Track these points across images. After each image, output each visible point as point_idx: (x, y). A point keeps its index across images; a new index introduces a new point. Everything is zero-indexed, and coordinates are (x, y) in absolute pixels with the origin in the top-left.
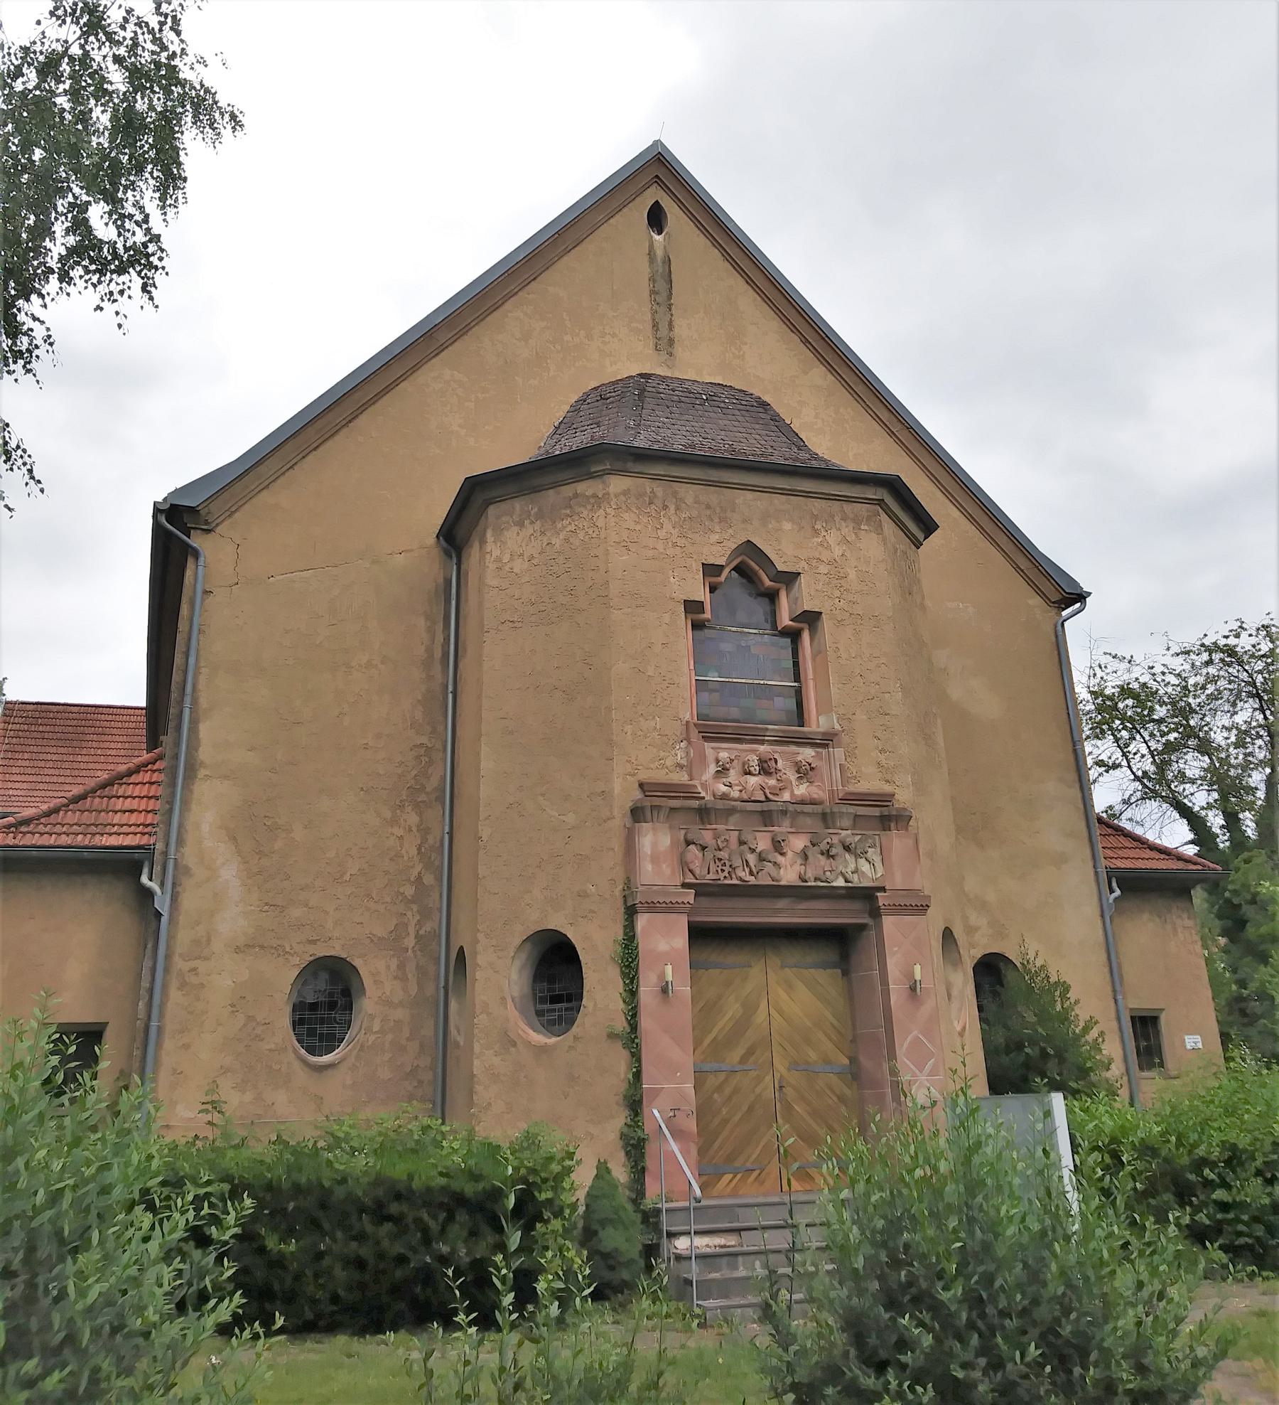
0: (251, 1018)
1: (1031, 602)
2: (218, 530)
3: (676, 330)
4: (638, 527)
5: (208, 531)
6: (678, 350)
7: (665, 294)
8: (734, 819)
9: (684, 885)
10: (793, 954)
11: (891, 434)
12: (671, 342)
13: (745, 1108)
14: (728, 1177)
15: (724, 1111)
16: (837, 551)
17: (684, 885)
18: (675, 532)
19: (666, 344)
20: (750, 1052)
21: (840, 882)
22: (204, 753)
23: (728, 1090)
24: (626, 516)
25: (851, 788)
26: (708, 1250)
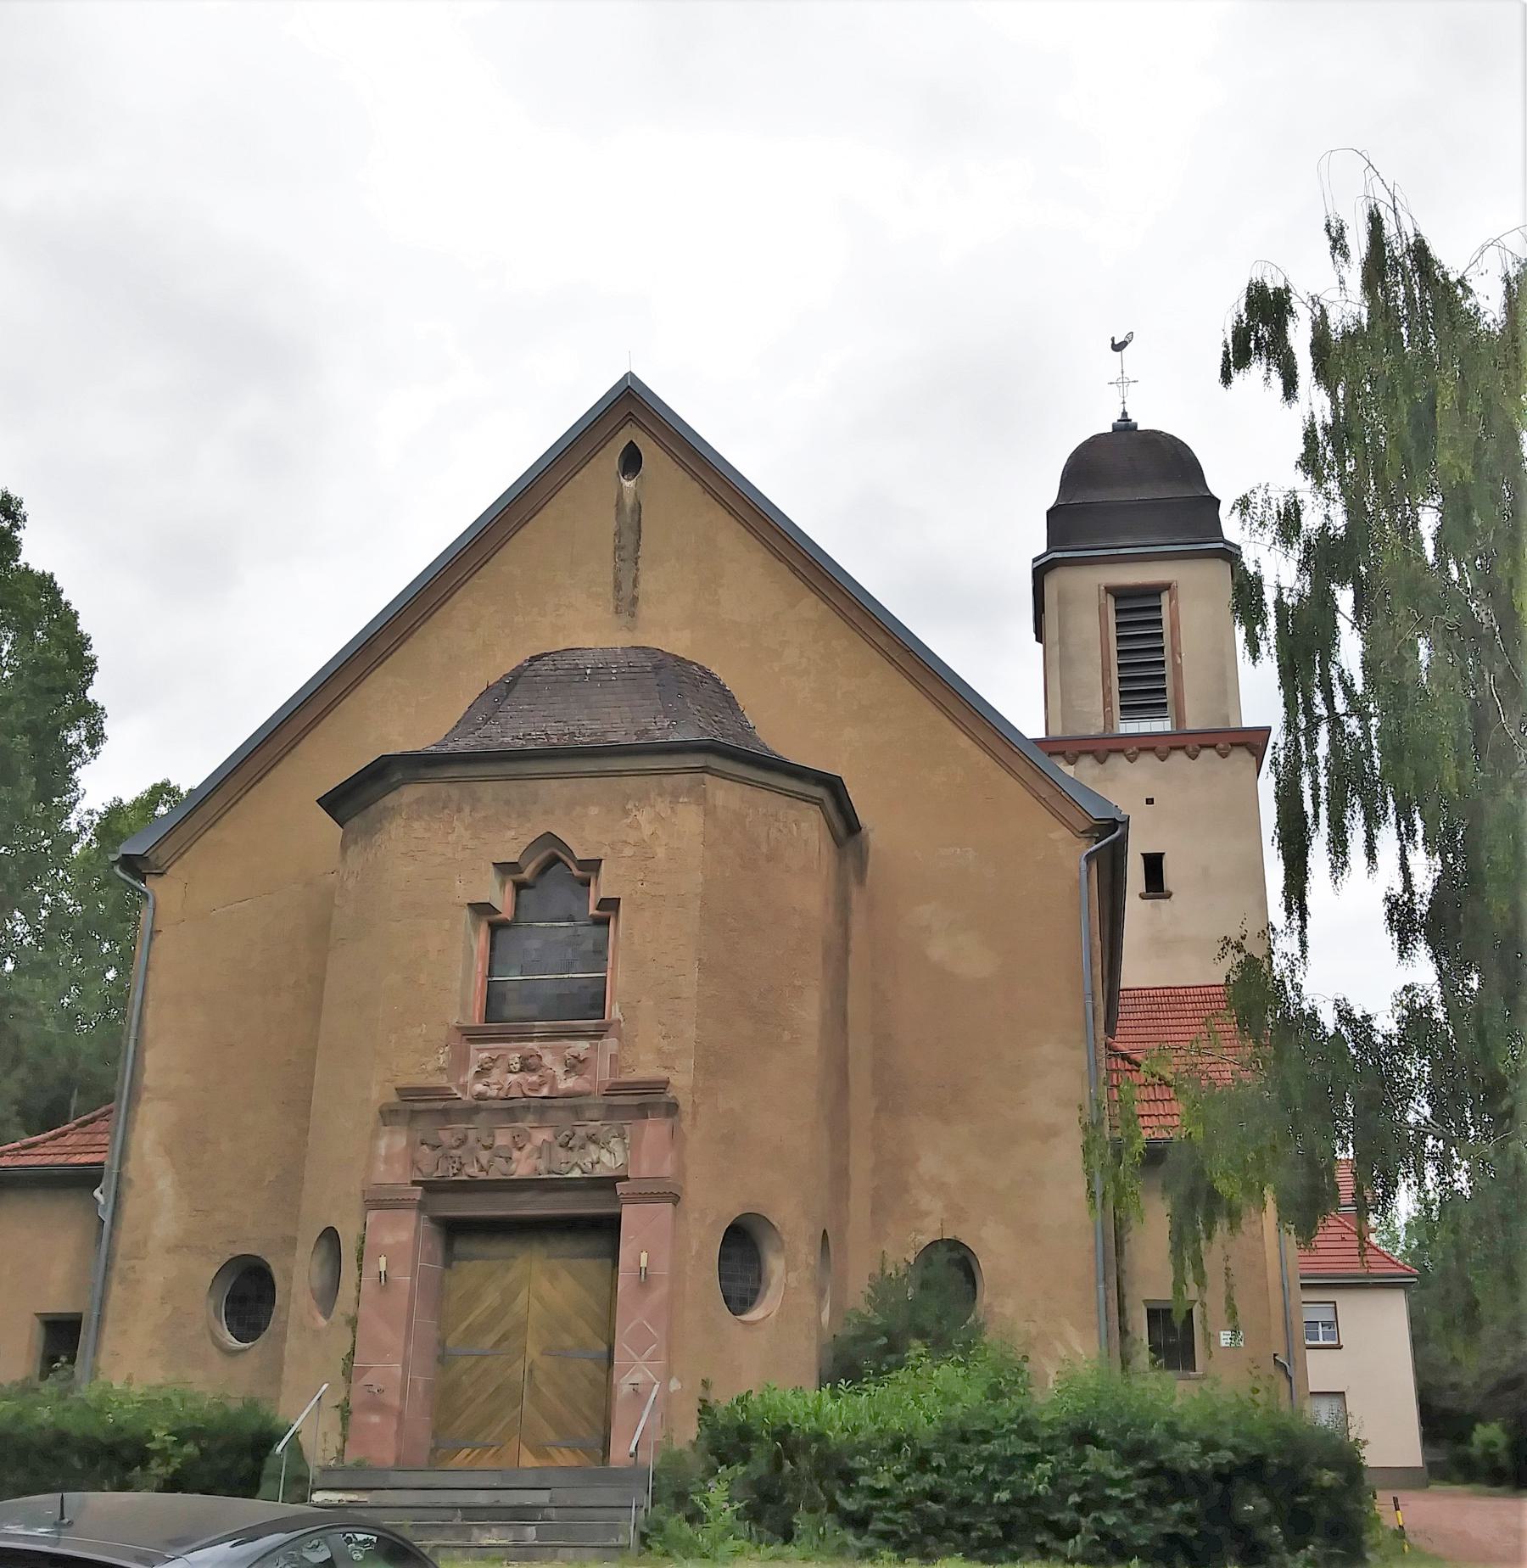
1: (1054, 836)
3: (642, 586)
4: (427, 835)
6: (644, 610)
7: (631, 548)
8: (480, 1118)
9: (414, 1183)
10: (567, 1245)
11: (892, 661)
12: (635, 600)
13: (491, 1390)
14: (467, 1451)
16: (647, 830)
17: (414, 1183)
18: (468, 834)
19: (627, 604)
20: (504, 1337)
21: (576, 1173)
22: (148, 1079)
24: (416, 825)
25: (624, 1078)
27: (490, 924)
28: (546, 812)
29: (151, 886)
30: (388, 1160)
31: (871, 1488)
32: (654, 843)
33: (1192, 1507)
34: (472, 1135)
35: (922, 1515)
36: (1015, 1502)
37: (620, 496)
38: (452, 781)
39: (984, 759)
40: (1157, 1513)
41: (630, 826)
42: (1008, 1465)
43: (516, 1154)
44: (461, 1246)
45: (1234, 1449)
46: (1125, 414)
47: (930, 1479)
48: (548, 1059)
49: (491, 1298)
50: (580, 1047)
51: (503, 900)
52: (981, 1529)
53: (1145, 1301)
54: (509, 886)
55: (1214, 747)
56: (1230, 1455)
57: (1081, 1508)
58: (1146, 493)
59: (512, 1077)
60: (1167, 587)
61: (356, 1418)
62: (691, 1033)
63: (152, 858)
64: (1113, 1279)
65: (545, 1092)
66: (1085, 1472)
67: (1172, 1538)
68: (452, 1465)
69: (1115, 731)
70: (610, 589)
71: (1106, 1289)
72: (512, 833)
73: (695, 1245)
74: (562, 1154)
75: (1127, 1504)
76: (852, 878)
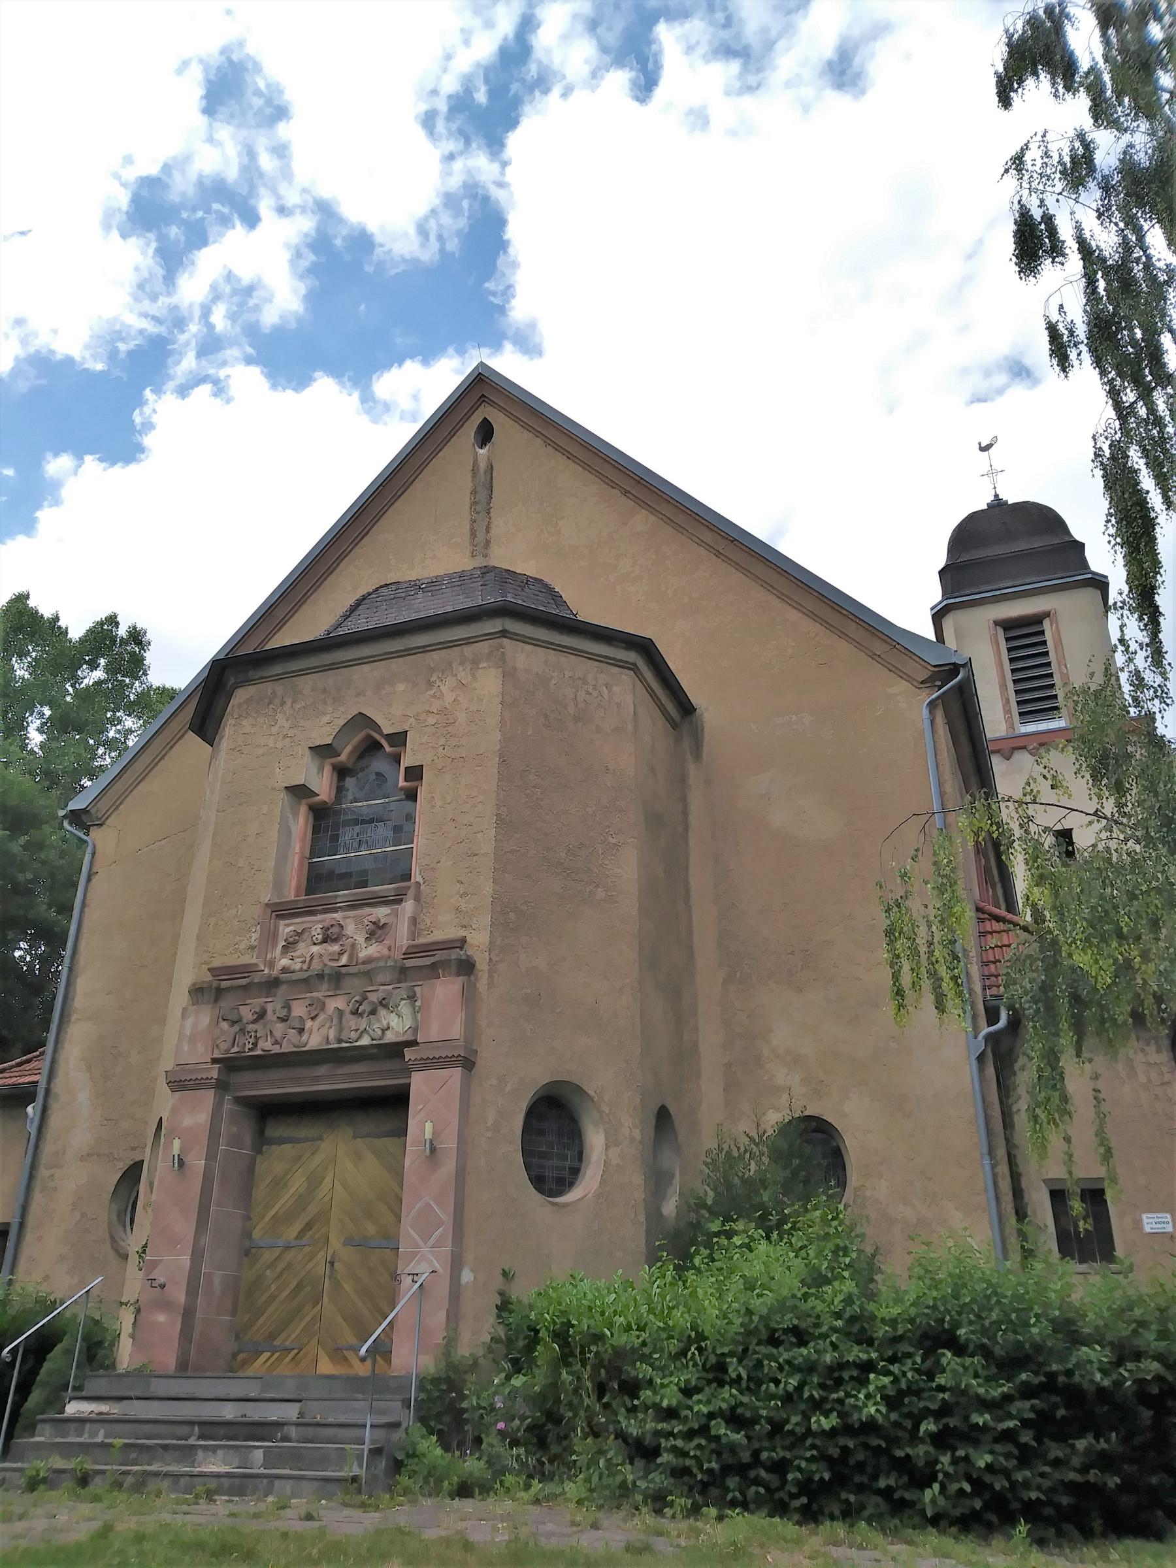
0: (84, 1214)
2: (107, 822)
5: (101, 825)
9: (215, 1061)
11: (718, 554)
12: (487, 543)
13: (293, 1285)
14: (266, 1355)
15: (273, 1287)
16: (449, 697)
20: (309, 1226)
21: (365, 1041)
23: (281, 1266)
24: (245, 722)
25: (416, 942)
26: (93, 1415)
27: (311, 808)
28: (358, 695)
29: (96, 836)
30: (192, 1040)
31: (657, 1407)
32: (455, 713)
33: (1111, 1442)
34: (269, 1007)
35: (719, 1448)
36: (847, 1429)
37: (475, 462)
38: (278, 678)
39: (815, 628)
40: (1056, 1451)
41: (434, 696)
42: (835, 1376)
43: (309, 1024)
44: (275, 1130)
45: (1159, 1358)
46: (996, 495)
47: (727, 1396)
48: (350, 928)
49: (298, 1183)
50: (381, 913)
51: (323, 785)
52: (799, 1469)
53: (1047, 1182)
54: (328, 769)
55: (1024, 748)
56: (1155, 1366)
57: (941, 1440)
58: (1020, 546)
59: (315, 949)
60: (1047, 615)
61: (143, 1314)
62: (488, 888)
63: (93, 811)
64: (1001, 1153)
65: (344, 960)
66: (941, 1389)
67: (1080, 1490)
68: (250, 1372)
69: (1017, 732)
70: (467, 538)
71: (993, 1167)
72: (327, 718)
73: (491, 1116)
74: (352, 1022)
75: (1008, 1436)
76: (689, 758)
